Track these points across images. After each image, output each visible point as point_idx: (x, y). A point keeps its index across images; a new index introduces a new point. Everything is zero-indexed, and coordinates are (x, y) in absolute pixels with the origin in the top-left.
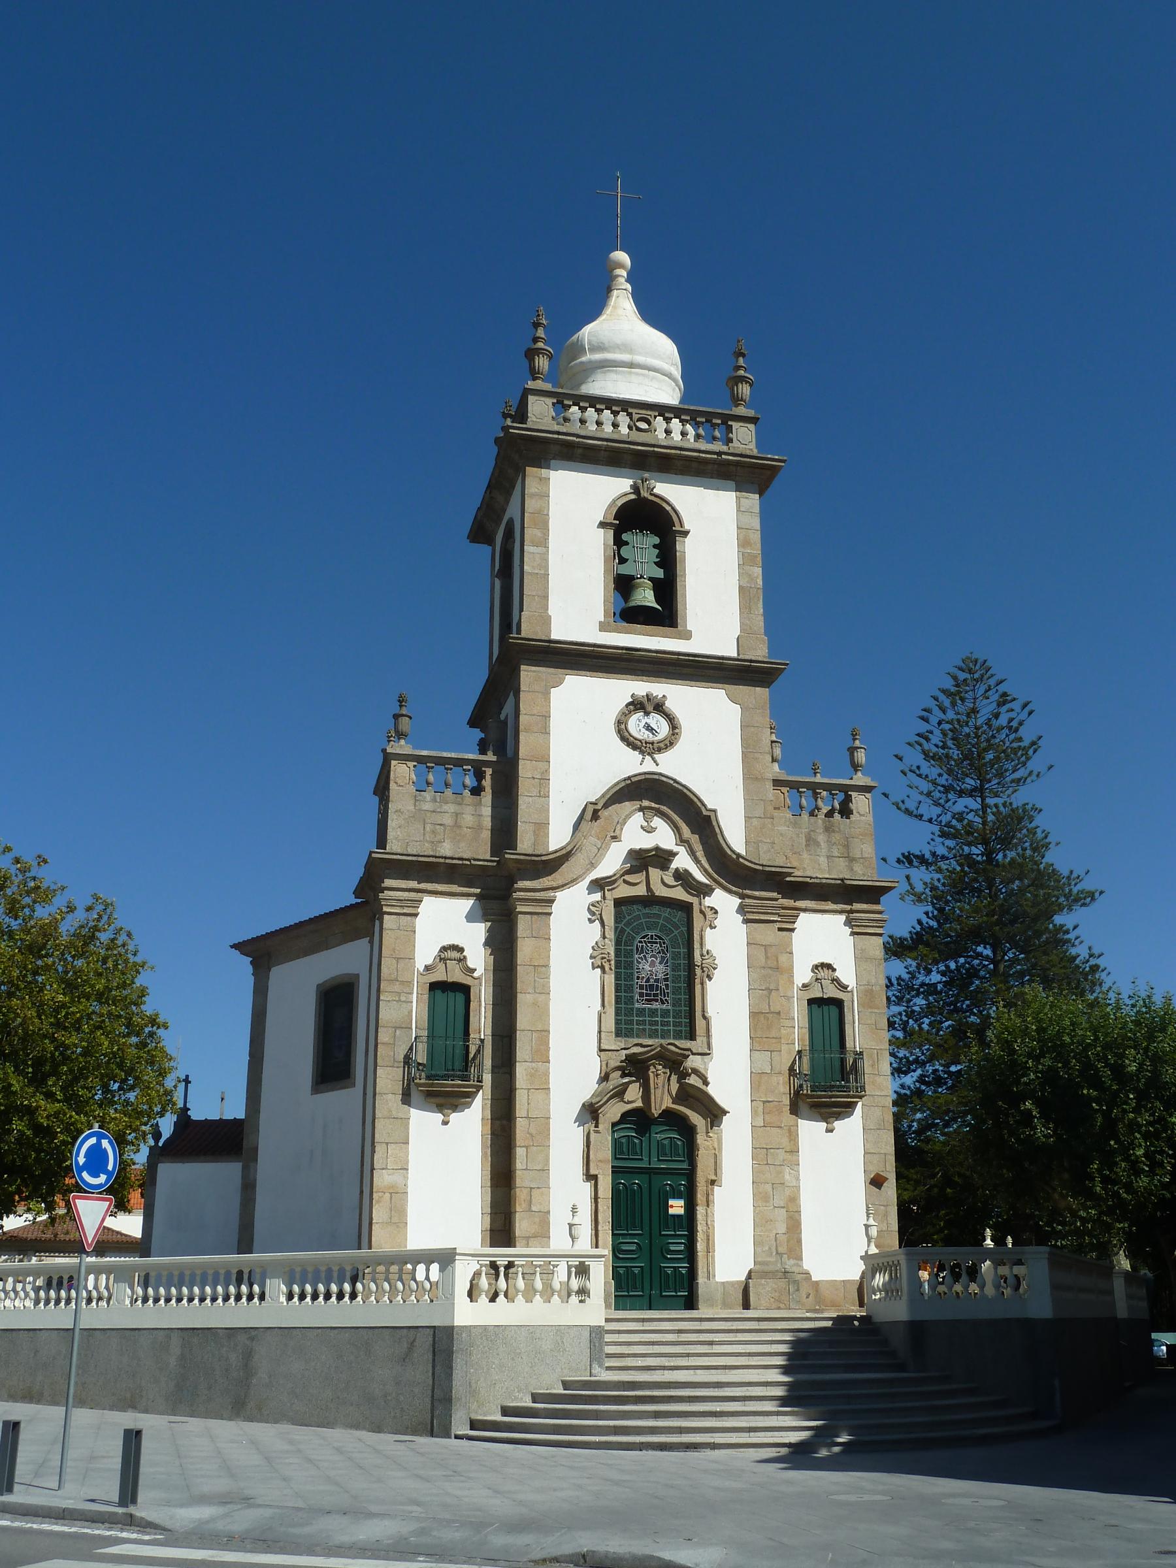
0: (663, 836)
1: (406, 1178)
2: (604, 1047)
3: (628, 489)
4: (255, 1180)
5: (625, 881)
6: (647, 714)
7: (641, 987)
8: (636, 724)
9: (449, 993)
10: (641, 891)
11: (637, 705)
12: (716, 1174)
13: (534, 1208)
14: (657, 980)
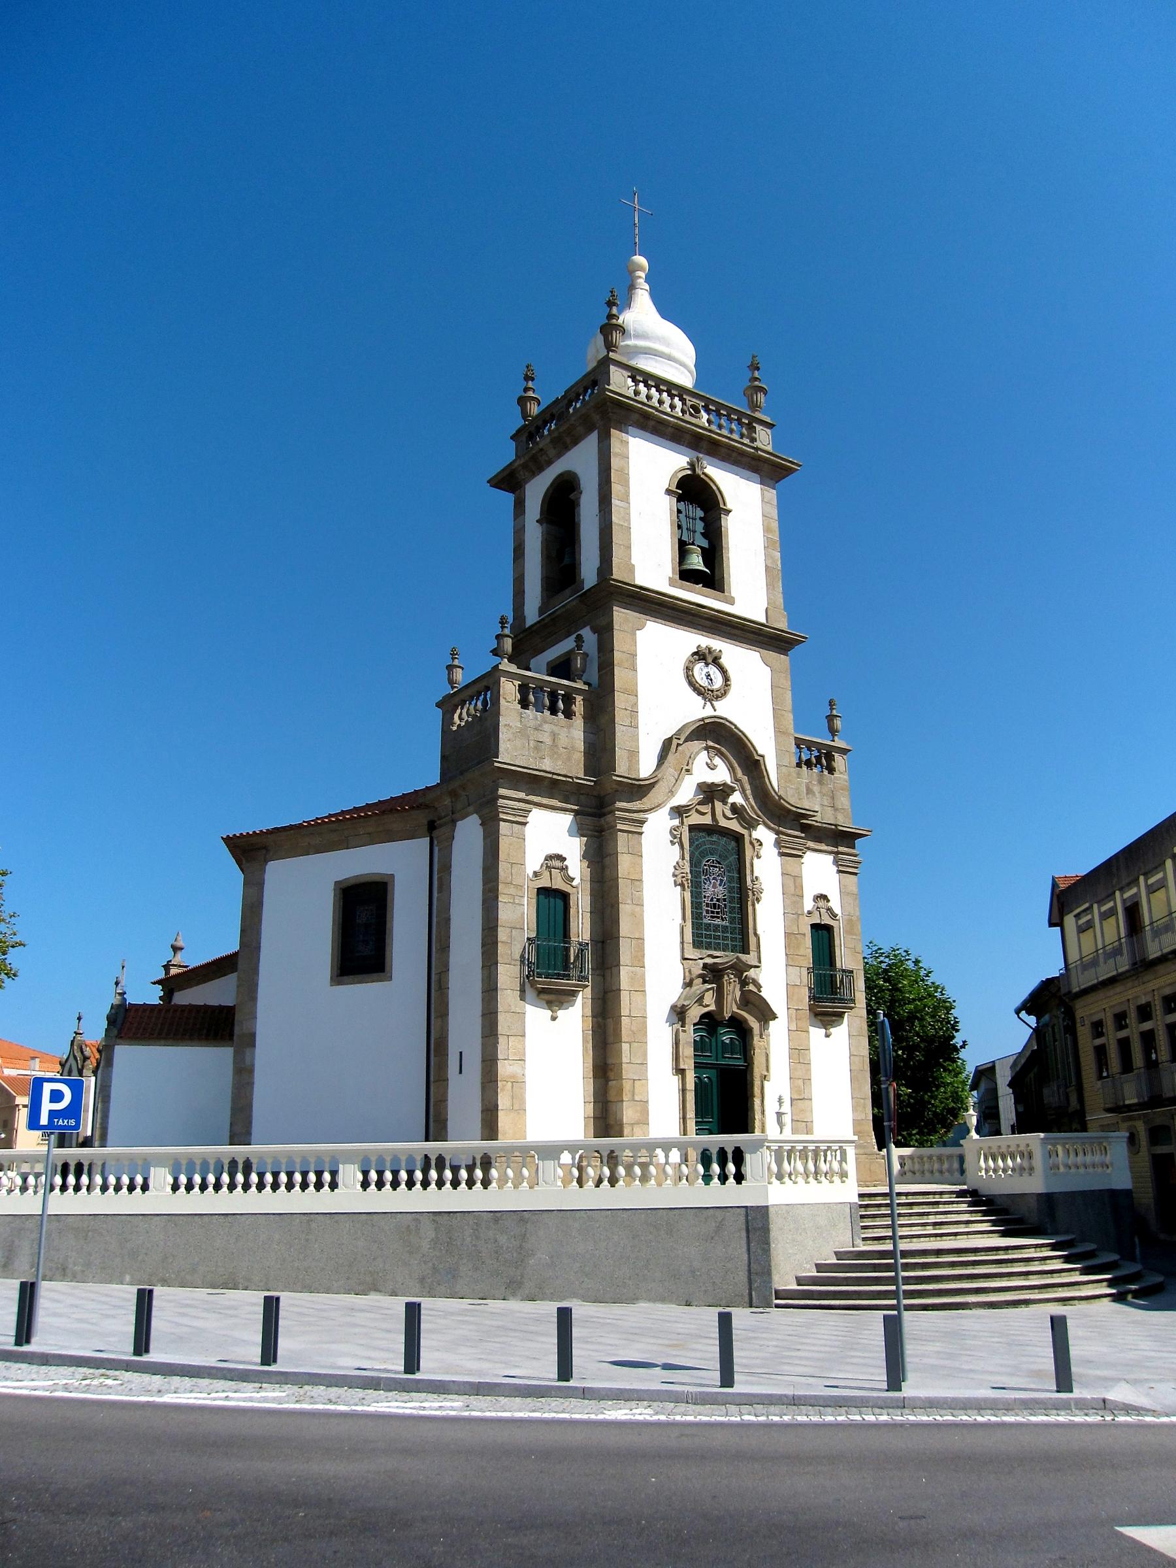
0: (721, 774)
1: (524, 1068)
2: (686, 956)
3: (685, 465)
4: (253, 1065)
5: (697, 811)
6: (707, 664)
7: (707, 905)
8: (700, 671)
9: (553, 901)
10: (707, 820)
11: (701, 656)
12: (768, 1070)
13: (637, 1098)
14: (718, 900)
